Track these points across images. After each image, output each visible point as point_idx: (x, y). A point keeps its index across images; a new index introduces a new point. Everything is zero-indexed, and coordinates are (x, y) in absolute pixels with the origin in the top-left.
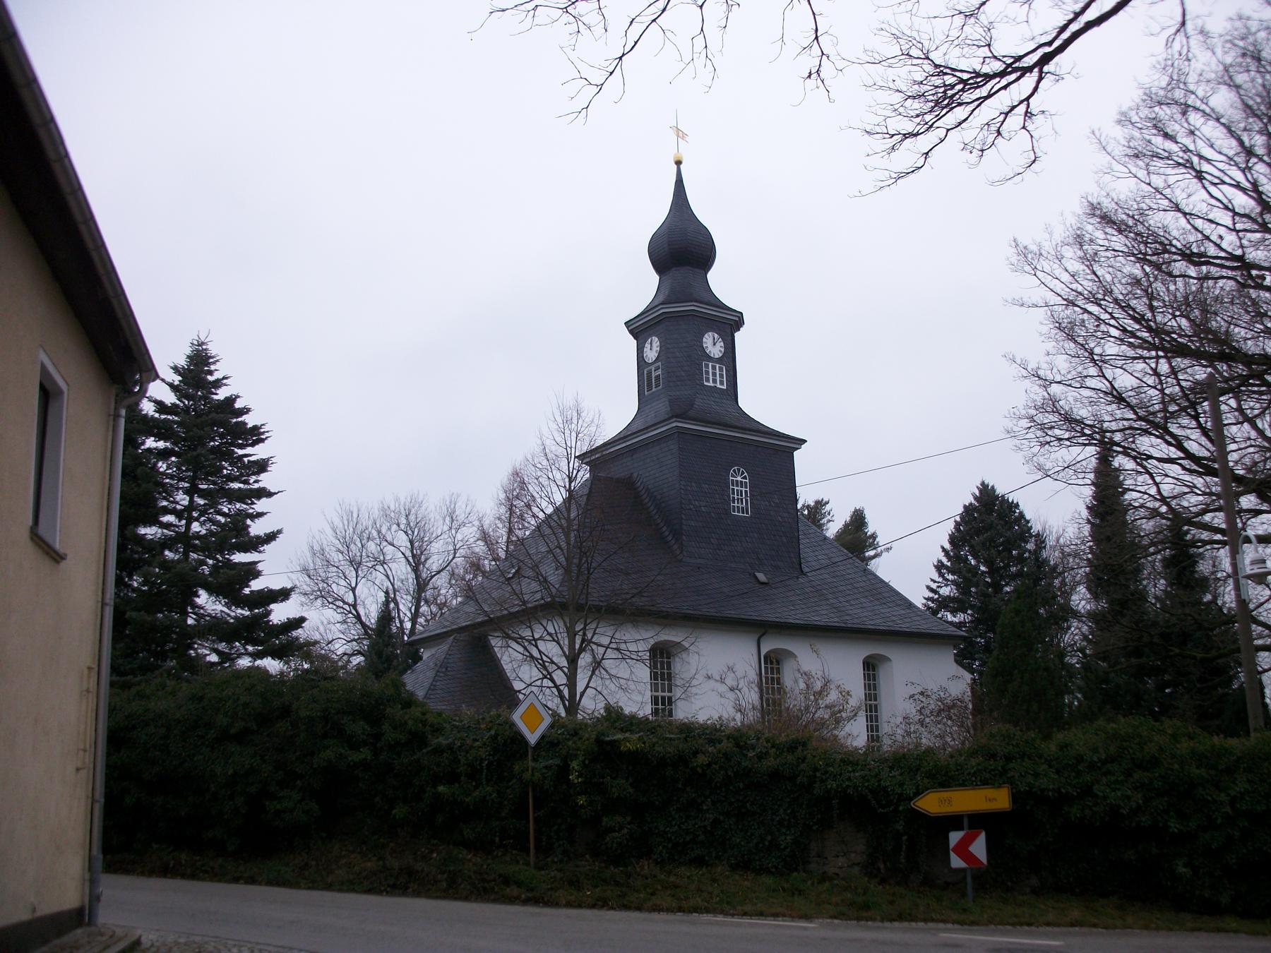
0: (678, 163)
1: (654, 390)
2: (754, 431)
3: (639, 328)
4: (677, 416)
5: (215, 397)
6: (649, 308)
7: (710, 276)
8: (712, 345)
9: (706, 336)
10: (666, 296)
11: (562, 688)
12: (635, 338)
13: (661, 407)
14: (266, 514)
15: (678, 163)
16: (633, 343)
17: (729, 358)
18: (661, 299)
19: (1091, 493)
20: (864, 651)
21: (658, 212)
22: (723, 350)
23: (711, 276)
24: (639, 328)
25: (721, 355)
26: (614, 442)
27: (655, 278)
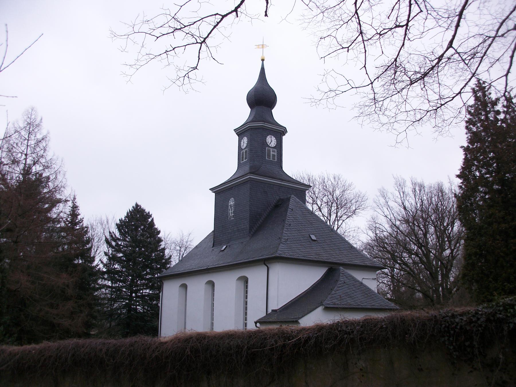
0: (263, 60)
1: (244, 161)
2: (287, 181)
3: (240, 132)
4: (250, 173)
5: (173, 263)
6: (246, 123)
7: (273, 111)
8: (271, 141)
9: (267, 139)
10: (253, 119)
11: (393, 32)
12: (238, 135)
13: (247, 169)
14: (54, 153)
15: (263, 60)
16: (237, 137)
17: (279, 146)
18: (251, 119)
19: (365, 241)
20: (204, 279)
21: (252, 82)
22: (276, 143)
23: (274, 111)
24: (240, 132)
25: (275, 146)
26: (245, 124)
27: (248, 110)
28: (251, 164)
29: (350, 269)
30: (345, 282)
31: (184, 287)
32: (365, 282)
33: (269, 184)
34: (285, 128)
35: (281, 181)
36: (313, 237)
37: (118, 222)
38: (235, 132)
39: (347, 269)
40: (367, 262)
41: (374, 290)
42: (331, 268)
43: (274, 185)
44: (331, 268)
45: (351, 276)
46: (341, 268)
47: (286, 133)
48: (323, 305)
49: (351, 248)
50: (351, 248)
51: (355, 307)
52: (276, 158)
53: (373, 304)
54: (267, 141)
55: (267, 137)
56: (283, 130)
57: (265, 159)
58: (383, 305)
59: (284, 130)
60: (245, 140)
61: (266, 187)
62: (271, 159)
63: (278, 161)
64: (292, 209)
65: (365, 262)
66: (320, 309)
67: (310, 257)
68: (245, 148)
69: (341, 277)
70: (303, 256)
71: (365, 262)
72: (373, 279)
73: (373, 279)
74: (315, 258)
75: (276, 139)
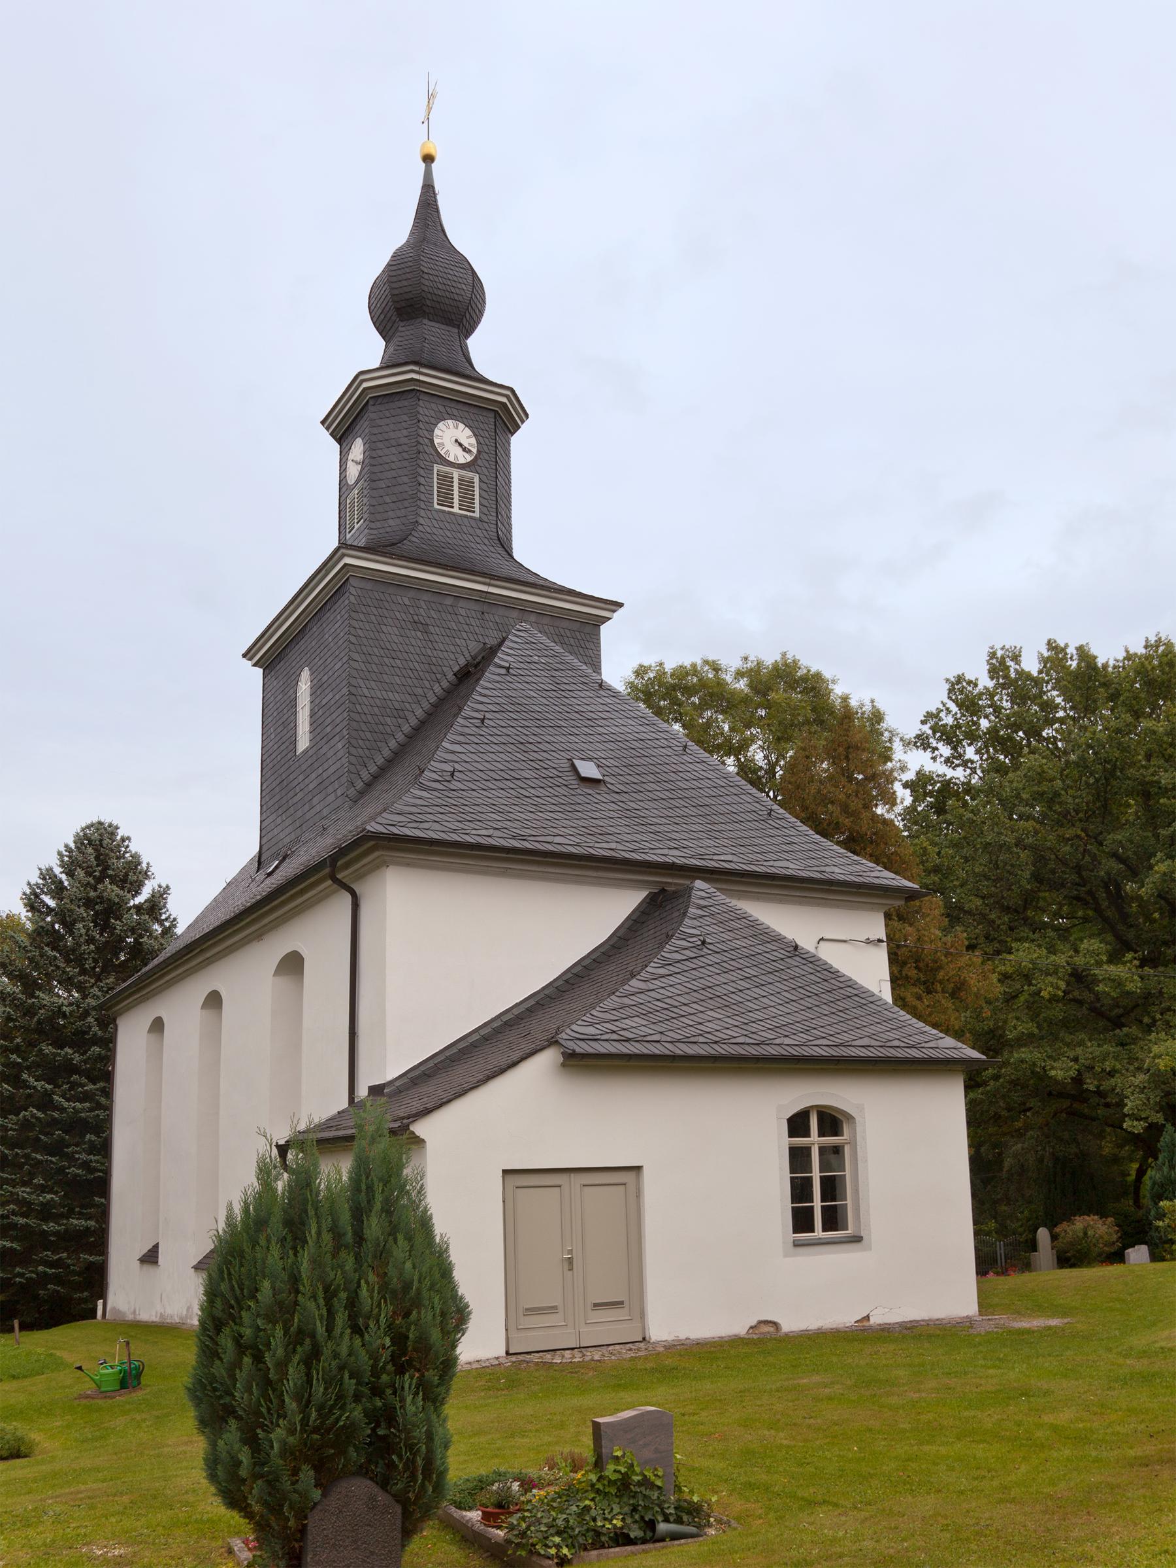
0: (428, 159)
15: (428, 159)
28: (375, 532)
29: (756, 897)
30: (704, 942)
31: (214, 1000)
32: (830, 955)
33: (439, 591)
34: (508, 393)
35: (488, 580)
36: (588, 769)
37: (121, 833)
38: (327, 429)
39: (731, 897)
40: (836, 870)
41: (876, 992)
42: (663, 891)
43: (460, 595)
44: (663, 891)
45: (744, 917)
46: (699, 884)
47: (523, 422)
48: (557, 1042)
49: (769, 814)
50: (769, 814)
51: (740, 1050)
52: (477, 505)
53: (845, 1037)
54: (436, 441)
55: (436, 425)
56: (504, 400)
57: (430, 508)
58: (896, 1043)
59: (507, 396)
60: (358, 450)
61: (423, 603)
62: (456, 510)
63: (485, 518)
64: (508, 669)
65: (827, 869)
66: (547, 1059)
67: (549, 839)
68: (357, 482)
69: (687, 921)
70: (514, 838)
71: (827, 869)
72: (868, 942)
73: (868, 942)
74: (578, 844)
75: (475, 435)
